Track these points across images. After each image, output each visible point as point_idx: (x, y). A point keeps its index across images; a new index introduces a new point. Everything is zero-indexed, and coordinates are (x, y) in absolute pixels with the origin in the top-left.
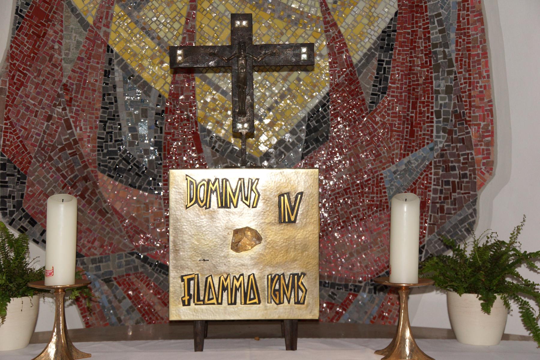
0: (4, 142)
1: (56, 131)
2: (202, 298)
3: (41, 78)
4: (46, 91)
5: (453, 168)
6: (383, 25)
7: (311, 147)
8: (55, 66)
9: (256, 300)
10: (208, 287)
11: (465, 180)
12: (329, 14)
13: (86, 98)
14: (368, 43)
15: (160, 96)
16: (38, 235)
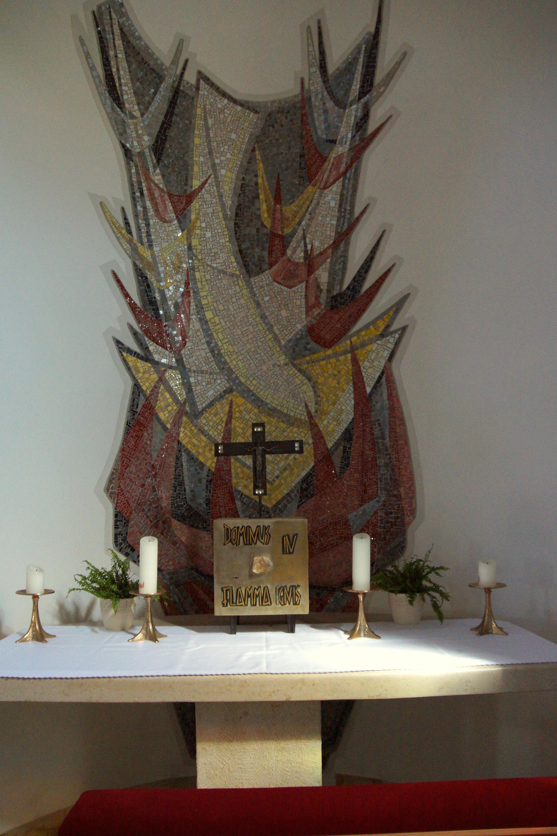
0: (117, 501)
1: (147, 493)
2: (235, 601)
3: (139, 462)
4: (142, 469)
5: (391, 513)
6: (345, 426)
7: (303, 501)
8: (147, 454)
9: (269, 603)
10: (238, 595)
11: (398, 520)
12: (313, 419)
13: (165, 472)
14: (337, 436)
15: (209, 470)
16: (136, 557)
